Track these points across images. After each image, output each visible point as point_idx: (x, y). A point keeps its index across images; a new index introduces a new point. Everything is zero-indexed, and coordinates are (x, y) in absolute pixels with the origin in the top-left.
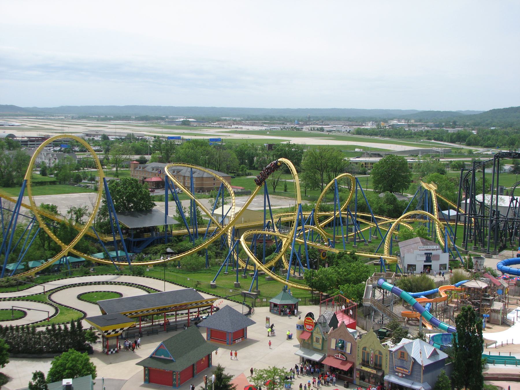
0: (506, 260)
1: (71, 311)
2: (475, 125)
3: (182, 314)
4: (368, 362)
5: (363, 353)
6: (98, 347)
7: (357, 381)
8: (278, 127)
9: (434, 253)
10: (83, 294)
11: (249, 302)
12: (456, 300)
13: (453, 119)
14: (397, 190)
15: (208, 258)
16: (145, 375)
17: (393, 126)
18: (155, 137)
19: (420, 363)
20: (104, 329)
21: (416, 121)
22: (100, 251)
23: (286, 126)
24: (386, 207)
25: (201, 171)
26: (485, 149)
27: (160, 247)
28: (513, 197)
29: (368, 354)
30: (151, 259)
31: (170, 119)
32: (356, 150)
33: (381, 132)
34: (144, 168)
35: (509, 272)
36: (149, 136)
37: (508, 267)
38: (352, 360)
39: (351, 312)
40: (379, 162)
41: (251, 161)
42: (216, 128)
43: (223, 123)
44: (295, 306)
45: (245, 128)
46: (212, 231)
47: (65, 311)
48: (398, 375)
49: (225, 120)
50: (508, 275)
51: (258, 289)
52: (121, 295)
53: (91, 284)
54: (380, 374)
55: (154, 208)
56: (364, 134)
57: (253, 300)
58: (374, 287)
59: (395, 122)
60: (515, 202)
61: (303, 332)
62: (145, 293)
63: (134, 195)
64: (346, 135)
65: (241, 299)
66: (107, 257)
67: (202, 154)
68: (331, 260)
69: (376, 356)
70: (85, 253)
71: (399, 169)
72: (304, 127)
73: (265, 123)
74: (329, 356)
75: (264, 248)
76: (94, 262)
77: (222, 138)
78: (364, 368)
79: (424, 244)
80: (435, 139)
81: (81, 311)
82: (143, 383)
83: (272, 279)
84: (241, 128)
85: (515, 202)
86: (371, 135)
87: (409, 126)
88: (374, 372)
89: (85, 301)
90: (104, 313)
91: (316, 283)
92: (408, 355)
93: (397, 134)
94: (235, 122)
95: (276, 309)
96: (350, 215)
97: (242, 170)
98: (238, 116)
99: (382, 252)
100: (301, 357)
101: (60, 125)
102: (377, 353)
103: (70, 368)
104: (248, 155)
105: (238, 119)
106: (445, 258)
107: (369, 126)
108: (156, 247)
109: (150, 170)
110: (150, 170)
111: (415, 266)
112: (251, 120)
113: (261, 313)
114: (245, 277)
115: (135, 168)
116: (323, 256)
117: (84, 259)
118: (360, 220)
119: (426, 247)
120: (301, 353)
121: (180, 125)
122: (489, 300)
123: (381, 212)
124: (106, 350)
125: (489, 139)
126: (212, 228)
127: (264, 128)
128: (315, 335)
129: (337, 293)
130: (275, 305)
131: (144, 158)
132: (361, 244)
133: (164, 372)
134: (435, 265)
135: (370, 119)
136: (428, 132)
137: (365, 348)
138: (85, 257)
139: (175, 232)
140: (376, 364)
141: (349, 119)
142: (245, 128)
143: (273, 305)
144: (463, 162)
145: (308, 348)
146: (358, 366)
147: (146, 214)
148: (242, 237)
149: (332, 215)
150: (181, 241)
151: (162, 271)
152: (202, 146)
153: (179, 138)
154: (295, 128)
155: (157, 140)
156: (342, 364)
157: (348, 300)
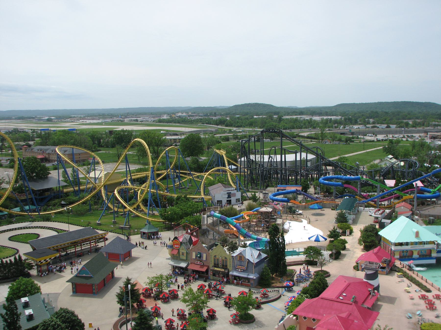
0: (274, 193)
1: (7, 249)
2: (227, 114)
3: (87, 244)
4: (218, 264)
5: (214, 259)
6: (34, 272)
7: (211, 277)
8: (109, 120)
9: (232, 192)
10: (12, 236)
11: (126, 232)
12: (255, 220)
13: (297, 109)
14: (197, 155)
15: (91, 205)
16: (73, 288)
17: (180, 116)
18: (32, 130)
19: (252, 262)
20: (38, 260)
21: (192, 113)
22: (16, 207)
23: (114, 119)
24: (193, 166)
25: (78, 150)
26: (237, 128)
27: (57, 201)
28: (270, 155)
29: (218, 260)
30: (52, 210)
31: (38, 118)
32: (162, 132)
33: (173, 120)
34: (32, 150)
35: (277, 200)
36: (27, 129)
37: (276, 197)
38: (207, 264)
39: (195, 234)
40: (184, 138)
41: (99, 142)
42: (69, 122)
43: (74, 119)
44: (156, 234)
45: (88, 121)
46: (89, 188)
47: (3, 249)
48: (238, 271)
49: (74, 117)
50: (277, 202)
51: (130, 224)
52: (38, 235)
53: (15, 229)
54: (227, 271)
55: (50, 175)
56: (163, 122)
57: (128, 231)
58: (208, 217)
59: (180, 114)
60: (271, 158)
61: (173, 249)
62: (55, 233)
63: (36, 168)
64: (152, 123)
65: (120, 231)
66: (22, 211)
67: (68, 138)
68: (171, 201)
69: (223, 260)
70: (8, 209)
71: (197, 142)
72: (126, 119)
73: (101, 118)
74: (191, 263)
75: (129, 197)
76: (14, 214)
77: (76, 128)
78: (216, 269)
79: (225, 188)
80: (207, 124)
81: (14, 249)
82: (72, 293)
83: (137, 216)
84: (86, 122)
85: (271, 158)
86: (168, 122)
87: (189, 116)
88: (223, 270)
89: (15, 241)
90: (34, 249)
91: (168, 217)
92: (244, 257)
93: (183, 121)
94: (81, 118)
95: (145, 235)
96: (175, 172)
97: (95, 148)
98: (82, 114)
99: (199, 193)
100: (172, 265)
101: (19, 124)
102: (224, 258)
103: (23, 290)
104: (97, 138)
105: (82, 116)
106: (238, 195)
107: (165, 117)
108: (54, 202)
109: (36, 151)
110: (36, 151)
111: (221, 201)
112: (91, 116)
113: (135, 239)
114: (118, 217)
115: (26, 150)
116: (165, 199)
117: (6, 213)
118: (181, 175)
119: (227, 189)
120: (172, 263)
121: (46, 121)
122: (274, 218)
123: (191, 169)
124: (40, 274)
125: (238, 122)
126: (90, 186)
127: (100, 121)
128: (181, 251)
129: (183, 221)
130: (144, 233)
131: (29, 143)
132: (183, 190)
133: (86, 285)
134: (233, 199)
135: (164, 113)
136: (201, 119)
137: (215, 256)
138: (6, 211)
139: (65, 190)
140: (223, 265)
141: (151, 114)
142: (88, 121)
143: (142, 233)
144: (228, 136)
145: (177, 259)
146: (211, 268)
147: (44, 180)
148: (116, 190)
149: (164, 172)
150: (68, 196)
151: (60, 216)
152: (69, 134)
153: (48, 130)
154: (120, 120)
155: (34, 131)
156: (200, 267)
157: (192, 226)
